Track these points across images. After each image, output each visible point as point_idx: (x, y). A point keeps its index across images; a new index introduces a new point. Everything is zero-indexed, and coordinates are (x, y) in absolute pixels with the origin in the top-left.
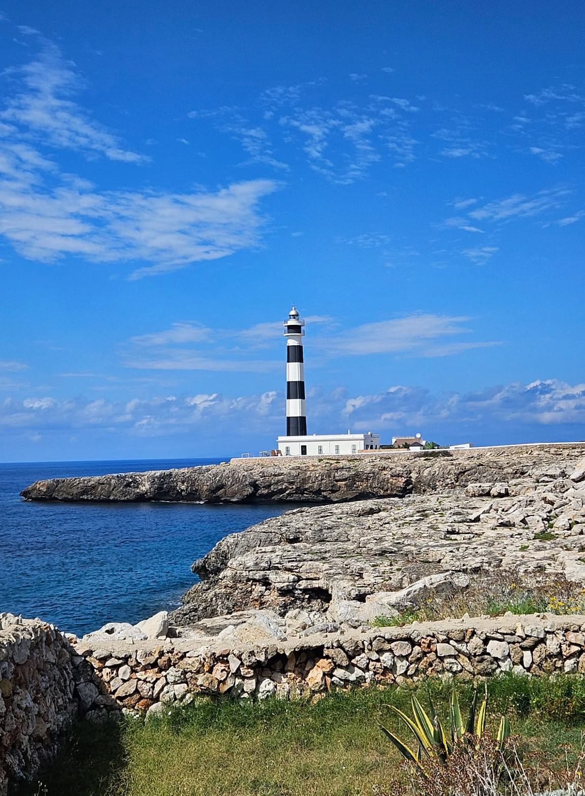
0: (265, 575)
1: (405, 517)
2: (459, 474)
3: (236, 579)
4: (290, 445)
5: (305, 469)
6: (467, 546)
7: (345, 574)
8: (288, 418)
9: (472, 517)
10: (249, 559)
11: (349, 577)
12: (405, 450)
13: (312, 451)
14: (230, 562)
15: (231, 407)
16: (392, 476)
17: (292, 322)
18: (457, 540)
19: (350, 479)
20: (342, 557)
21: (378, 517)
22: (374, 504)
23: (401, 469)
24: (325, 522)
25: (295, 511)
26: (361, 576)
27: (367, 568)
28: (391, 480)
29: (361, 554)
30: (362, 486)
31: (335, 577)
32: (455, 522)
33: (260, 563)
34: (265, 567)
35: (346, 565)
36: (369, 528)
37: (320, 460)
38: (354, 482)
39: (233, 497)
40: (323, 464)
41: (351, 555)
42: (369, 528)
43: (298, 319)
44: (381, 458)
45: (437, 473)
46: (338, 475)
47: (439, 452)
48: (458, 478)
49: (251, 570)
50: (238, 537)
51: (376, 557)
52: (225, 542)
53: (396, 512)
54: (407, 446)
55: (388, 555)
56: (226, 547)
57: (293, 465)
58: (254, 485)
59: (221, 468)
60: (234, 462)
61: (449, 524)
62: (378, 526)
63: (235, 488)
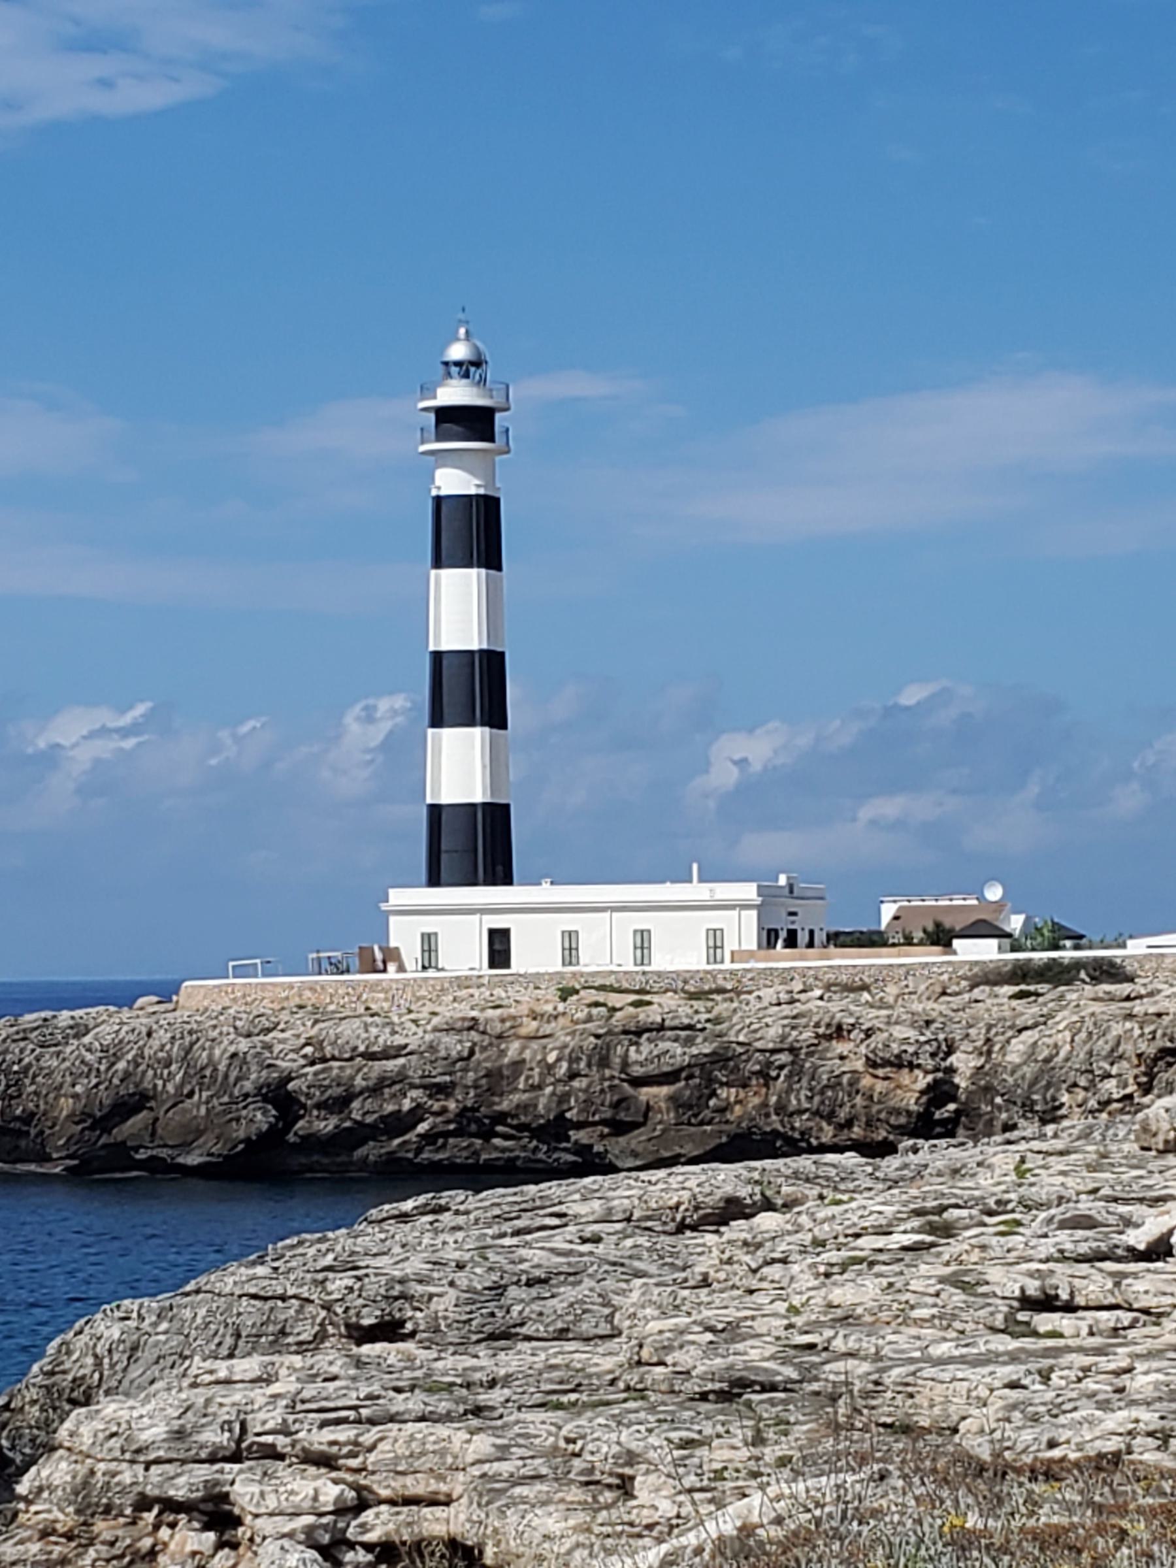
0: (217, 1483)
1: (857, 1236)
2: (1156, 1060)
3: (90, 1502)
4: (440, 928)
5: (498, 1028)
6: (1087, 1360)
7: (562, 1479)
8: (435, 811)
9: (1138, 1238)
10: (149, 1416)
11: (575, 1494)
12: (932, 956)
13: (535, 952)
14: (68, 1425)
15: (213, 762)
16: (872, 1064)
17: (456, 393)
18: (1061, 1336)
19: (690, 1077)
20: (559, 1406)
21: (744, 1235)
22: (749, 1181)
23: (912, 1034)
24: (523, 1252)
25: (408, 1205)
26: (625, 1487)
27: (652, 1455)
28: (866, 1081)
29: (639, 1393)
30: (742, 1104)
31: (518, 1490)
32: (1062, 1257)
33: (198, 1428)
34: (218, 1448)
35: (569, 1441)
36: (705, 1282)
37: (566, 994)
38: (709, 1087)
39: (185, 1146)
40: (576, 1008)
41: (602, 1396)
42: (705, 1282)
43: (482, 381)
44: (828, 987)
45: (1063, 1054)
46: (641, 1054)
47: (1078, 965)
48: (1151, 1076)
49: (158, 1461)
50: (141, 1318)
51: (704, 1407)
52: (84, 1338)
53: (820, 1215)
54: (941, 937)
55: (756, 1397)
56: (90, 1360)
57: (449, 1011)
58: (280, 1097)
59: (135, 1023)
60: (197, 994)
61: (1035, 1266)
62: (741, 1270)
63: (197, 1107)
